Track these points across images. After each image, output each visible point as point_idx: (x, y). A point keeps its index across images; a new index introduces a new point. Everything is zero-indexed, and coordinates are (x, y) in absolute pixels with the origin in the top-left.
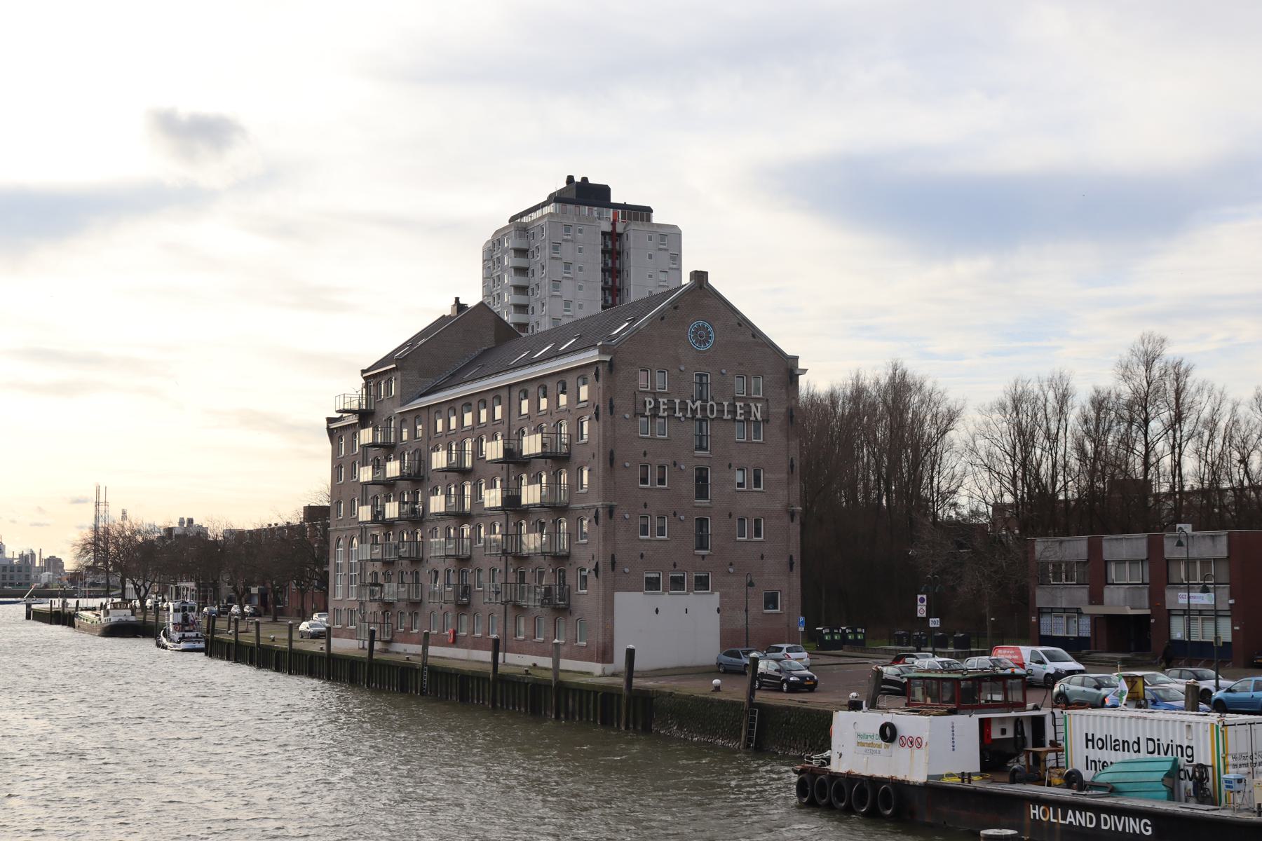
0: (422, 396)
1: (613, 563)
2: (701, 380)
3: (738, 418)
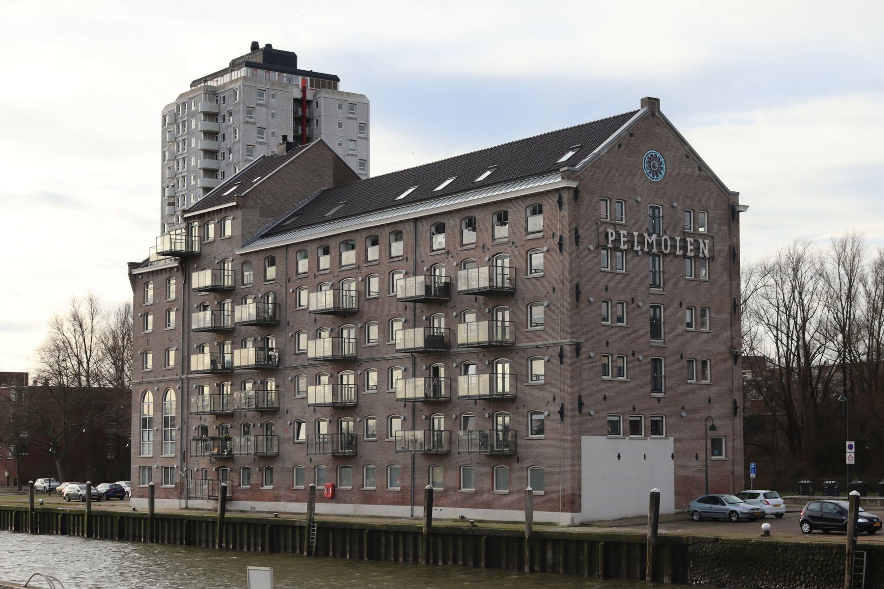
0: (264, 236)
1: (581, 404)
2: (654, 212)
3: (689, 254)
